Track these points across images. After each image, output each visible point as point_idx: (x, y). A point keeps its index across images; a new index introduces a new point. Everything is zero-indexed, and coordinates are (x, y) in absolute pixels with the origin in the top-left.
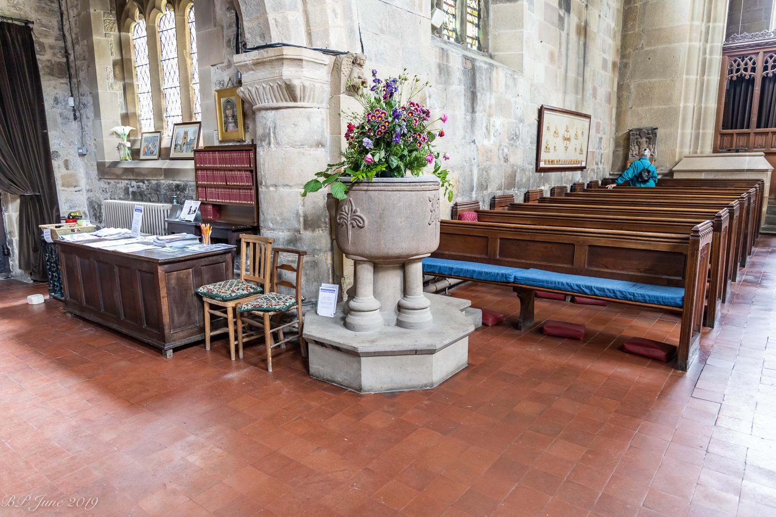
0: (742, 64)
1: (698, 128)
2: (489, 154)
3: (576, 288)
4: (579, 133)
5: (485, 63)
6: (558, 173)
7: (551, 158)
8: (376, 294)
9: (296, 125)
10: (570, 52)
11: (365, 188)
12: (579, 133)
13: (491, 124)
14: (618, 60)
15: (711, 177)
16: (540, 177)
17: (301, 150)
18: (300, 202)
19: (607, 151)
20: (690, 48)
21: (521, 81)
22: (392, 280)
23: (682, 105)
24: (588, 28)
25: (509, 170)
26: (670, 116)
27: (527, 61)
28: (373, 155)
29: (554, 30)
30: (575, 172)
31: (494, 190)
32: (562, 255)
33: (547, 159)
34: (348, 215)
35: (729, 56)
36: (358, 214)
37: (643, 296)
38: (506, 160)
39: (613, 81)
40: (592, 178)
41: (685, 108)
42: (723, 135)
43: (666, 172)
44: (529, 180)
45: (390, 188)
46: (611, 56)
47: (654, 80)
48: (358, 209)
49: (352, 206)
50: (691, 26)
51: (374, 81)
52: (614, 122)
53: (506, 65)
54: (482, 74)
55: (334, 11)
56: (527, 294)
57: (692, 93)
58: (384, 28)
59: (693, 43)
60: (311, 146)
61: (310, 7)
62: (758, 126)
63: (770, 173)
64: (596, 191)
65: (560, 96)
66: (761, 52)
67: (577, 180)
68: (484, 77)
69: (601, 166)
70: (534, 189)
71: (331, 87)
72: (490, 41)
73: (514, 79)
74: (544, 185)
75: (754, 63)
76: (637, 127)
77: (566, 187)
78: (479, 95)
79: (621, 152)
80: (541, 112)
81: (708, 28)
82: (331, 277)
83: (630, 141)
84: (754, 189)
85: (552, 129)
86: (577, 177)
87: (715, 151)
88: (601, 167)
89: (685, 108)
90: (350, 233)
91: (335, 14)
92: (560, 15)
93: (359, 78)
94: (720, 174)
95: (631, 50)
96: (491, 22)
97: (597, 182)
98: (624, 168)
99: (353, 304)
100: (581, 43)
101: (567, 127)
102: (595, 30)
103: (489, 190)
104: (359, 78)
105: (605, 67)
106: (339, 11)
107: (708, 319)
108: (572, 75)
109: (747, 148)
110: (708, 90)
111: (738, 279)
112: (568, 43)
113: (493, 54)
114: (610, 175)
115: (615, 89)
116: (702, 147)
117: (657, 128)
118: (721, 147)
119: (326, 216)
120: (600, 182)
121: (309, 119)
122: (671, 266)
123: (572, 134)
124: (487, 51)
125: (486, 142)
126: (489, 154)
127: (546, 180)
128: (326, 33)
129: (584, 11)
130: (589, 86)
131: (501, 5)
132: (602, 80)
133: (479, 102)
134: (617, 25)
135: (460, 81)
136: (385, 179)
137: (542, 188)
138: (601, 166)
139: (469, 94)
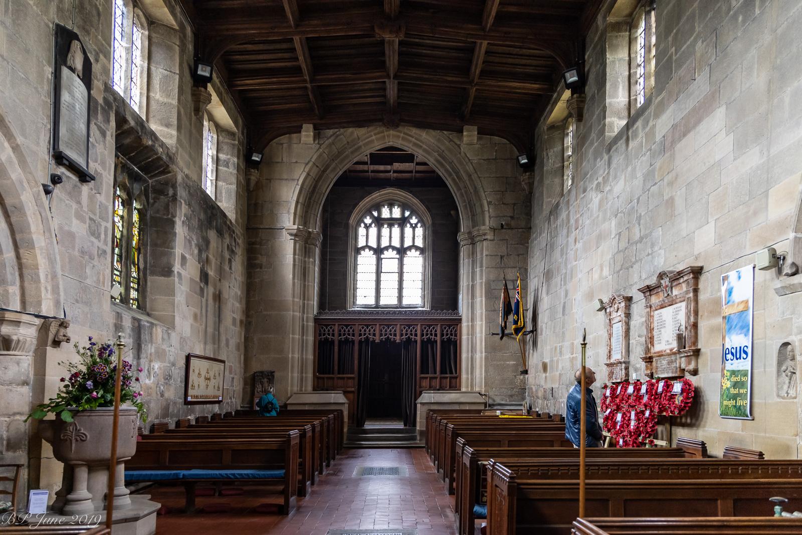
0: (327, 330)
1: (302, 373)
2: (150, 390)
3: (225, 476)
4: (217, 375)
5: (148, 322)
6: (201, 406)
7: (196, 394)
8: (89, 489)
9: (6, 368)
10: (209, 313)
11: (89, 414)
12: (217, 375)
13: (152, 367)
14: (244, 319)
15: (311, 408)
16: (188, 409)
17: (10, 387)
18: (4, 428)
19: (238, 388)
20: (293, 316)
21: (173, 335)
22: (102, 479)
23: (290, 356)
24: (221, 296)
25: (165, 403)
26: (283, 362)
27: (178, 320)
28: (97, 393)
29: (197, 297)
30: (214, 405)
31: (152, 419)
32: (213, 458)
33: (193, 394)
34: (72, 432)
35: (319, 324)
36: (82, 431)
37: (264, 475)
38: (162, 395)
39: (241, 334)
40: (227, 410)
41: (293, 357)
42: (318, 378)
43: (282, 404)
44: (179, 411)
45: (107, 414)
46: (238, 316)
47: (270, 336)
48: (82, 429)
49: (76, 426)
50: (293, 301)
51: (90, 344)
52: (242, 365)
53: (161, 322)
54: (145, 330)
55: (46, 288)
56: (189, 485)
57: (297, 347)
58: (78, 298)
59: (295, 313)
60: (18, 385)
61: (26, 284)
62: (339, 373)
63: (347, 405)
64: (230, 420)
65: (202, 346)
66: (337, 324)
67: (216, 411)
68: (146, 333)
69: (234, 400)
70: (183, 418)
71: (37, 341)
72: (147, 303)
73: (168, 333)
74: (190, 415)
75: (333, 331)
76: (260, 370)
77: (207, 417)
78: (143, 345)
79: (249, 389)
80: (188, 358)
81: (304, 304)
82: (26, 490)
83: (256, 380)
84: (332, 415)
85: (197, 372)
86: (216, 408)
87: (314, 389)
88: (234, 403)
89: (293, 357)
90: (74, 445)
91: (47, 290)
92: (201, 287)
93: (64, 336)
94: (318, 406)
95: (253, 312)
96: (149, 289)
97: (231, 413)
98: (251, 402)
99: (70, 497)
100: (217, 306)
101: (208, 370)
102: (227, 297)
103: (149, 419)
104: (64, 336)
105: (234, 324)
106: (49, 288)
107: (301, 493)
108: (210, 330)
109: (333, 388)
110: (307, 346)
111: (324, 473)
112: (207, 306)
113: (150, 312)
114: (241, 407)
115: (243, 340)
116: (306, 387)
117: (274, 372)
118: (319, 387)
119: (26, 440)
120: (233, 413)
121: (18, 364)
122: (277, 457)
123: (211, 374)
124: (145, 310)
125: (147, 381)
126: (150, 390)
127: (192, 412)
128: (39, 303)
129: (218, 284)
130: (223, 338)
131: (157, 277)
132: (232, 333)
133: (143, 351)
134: (242, 293)
135: (130, 336)
136: (104, 408)
137: (189, 417)
138: (234, 400)
139: (136, 346)
